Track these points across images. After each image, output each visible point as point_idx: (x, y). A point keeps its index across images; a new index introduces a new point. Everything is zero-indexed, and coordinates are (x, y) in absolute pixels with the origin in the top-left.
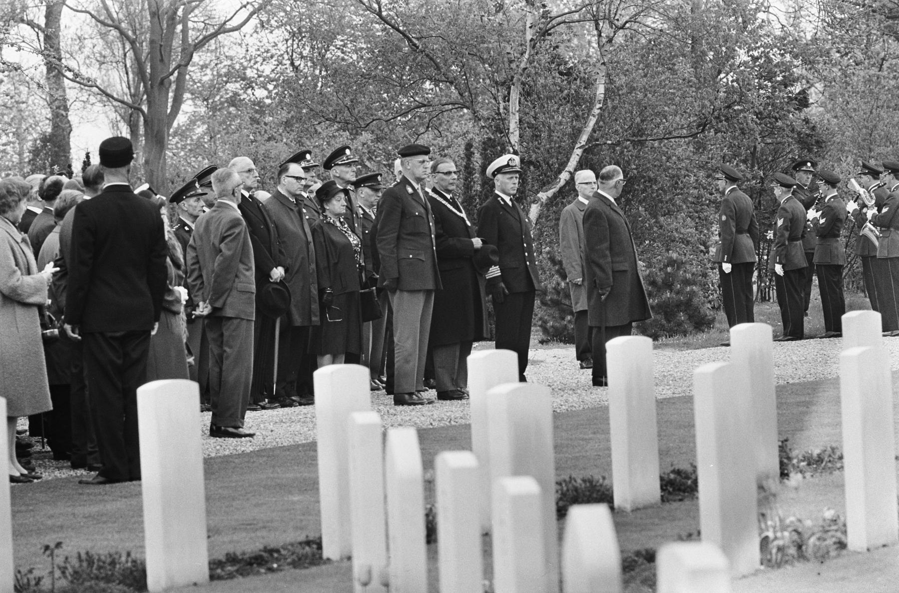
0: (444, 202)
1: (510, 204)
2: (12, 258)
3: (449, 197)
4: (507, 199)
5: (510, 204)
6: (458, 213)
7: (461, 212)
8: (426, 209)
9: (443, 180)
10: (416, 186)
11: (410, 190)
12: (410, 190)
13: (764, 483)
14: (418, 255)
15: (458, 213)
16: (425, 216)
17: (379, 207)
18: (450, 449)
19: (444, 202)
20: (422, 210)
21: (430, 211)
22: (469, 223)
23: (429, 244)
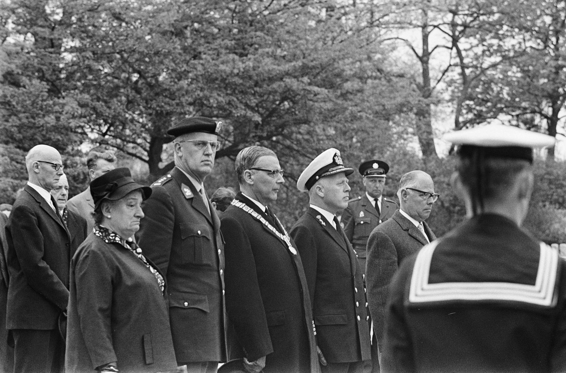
0: (255, 214)
1: (334, 225)
2: (333, 237)
3: (263, 209)
4: (330, 217)
5: (334, 225)
6: (277, 233)
7: (284, 234)
8: (212, 225)
9: (265, 182)
10: (199, 187)
11: (188, 193)
12: (188, 193)
13: (380, 66)
14: (200, 301)
15: (277, 233)
16: (210, 237)
17: (12, 211)
18: (409, 295)
19: (255, 214)
20: (208, 228)
21: (219, 231)
22: (293, 251)
23: (215, 284)
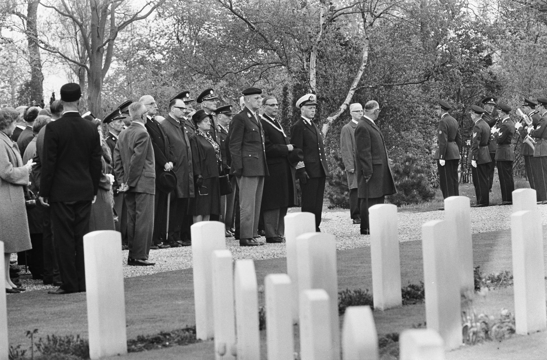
0: (270, 123)
1: (310, 124)
2: (7, 157)
3: (273, 119)
4: (309, 121)
5: (310, 124)
6: (279, 129)
7: (280, 128)
8: (259, 127)
9: (269, 109)
10: (253, 113)
11: (249, 115)
12: (249, 115)
13: (465, 294)
14: (254, 155)
15: (279, 129)
16: (258, 131)
17: (231, 125)
18: (274, 273)
19: (270, 123)
20: (257, 128)
21: (262, 128)
22: (285, 136)
23: (261, 148)
